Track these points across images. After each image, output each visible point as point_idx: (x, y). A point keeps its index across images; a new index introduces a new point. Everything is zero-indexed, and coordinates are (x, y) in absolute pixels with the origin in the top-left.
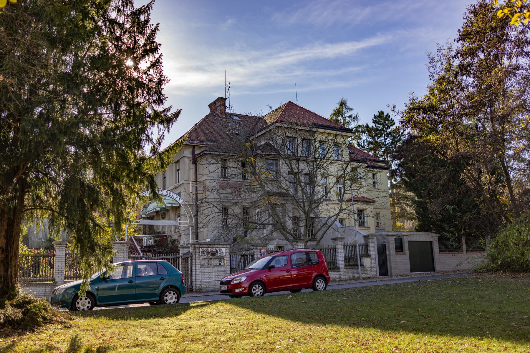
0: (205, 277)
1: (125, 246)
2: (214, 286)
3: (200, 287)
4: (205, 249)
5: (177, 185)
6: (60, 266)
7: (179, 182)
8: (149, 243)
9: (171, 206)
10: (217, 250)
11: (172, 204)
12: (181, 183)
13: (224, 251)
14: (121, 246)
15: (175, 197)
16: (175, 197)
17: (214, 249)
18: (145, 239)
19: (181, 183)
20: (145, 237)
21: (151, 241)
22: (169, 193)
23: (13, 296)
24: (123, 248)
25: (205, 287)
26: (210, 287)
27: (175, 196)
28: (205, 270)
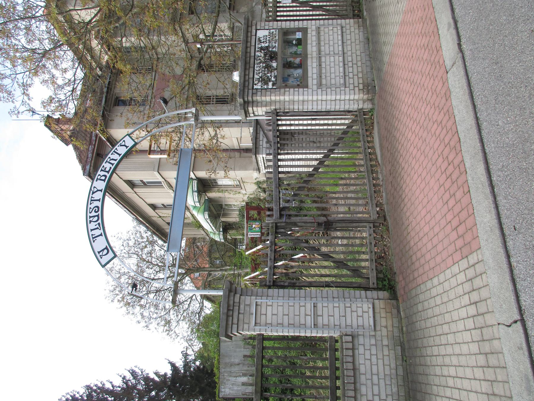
0: (333, 76)
1: (237, 300)
2: (358, 53)
3: (361, 86)
4: (256, 77)
5: (164, 184)
6: (275, 312)
7: (160, 182)
8: (257, 229)
9: (196, 194)
10: (262, 49)
11: (193, 192)
12: (161, 179)
13: (266, 33)
14: (236, 314)
15: (116, 157)
16: (116, 157)
17: (258, 54)
18: (251, 235)
19: (161, 179)
20: (247, 235)
21: (254, 226)
22: (103, 173)
23: (234, 84)
24: (242, 306)
25: (360, 75)
26: (359, 64)
27: (112, 157)
28: (315, 76)
